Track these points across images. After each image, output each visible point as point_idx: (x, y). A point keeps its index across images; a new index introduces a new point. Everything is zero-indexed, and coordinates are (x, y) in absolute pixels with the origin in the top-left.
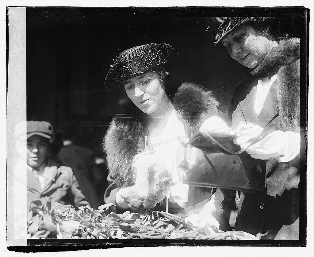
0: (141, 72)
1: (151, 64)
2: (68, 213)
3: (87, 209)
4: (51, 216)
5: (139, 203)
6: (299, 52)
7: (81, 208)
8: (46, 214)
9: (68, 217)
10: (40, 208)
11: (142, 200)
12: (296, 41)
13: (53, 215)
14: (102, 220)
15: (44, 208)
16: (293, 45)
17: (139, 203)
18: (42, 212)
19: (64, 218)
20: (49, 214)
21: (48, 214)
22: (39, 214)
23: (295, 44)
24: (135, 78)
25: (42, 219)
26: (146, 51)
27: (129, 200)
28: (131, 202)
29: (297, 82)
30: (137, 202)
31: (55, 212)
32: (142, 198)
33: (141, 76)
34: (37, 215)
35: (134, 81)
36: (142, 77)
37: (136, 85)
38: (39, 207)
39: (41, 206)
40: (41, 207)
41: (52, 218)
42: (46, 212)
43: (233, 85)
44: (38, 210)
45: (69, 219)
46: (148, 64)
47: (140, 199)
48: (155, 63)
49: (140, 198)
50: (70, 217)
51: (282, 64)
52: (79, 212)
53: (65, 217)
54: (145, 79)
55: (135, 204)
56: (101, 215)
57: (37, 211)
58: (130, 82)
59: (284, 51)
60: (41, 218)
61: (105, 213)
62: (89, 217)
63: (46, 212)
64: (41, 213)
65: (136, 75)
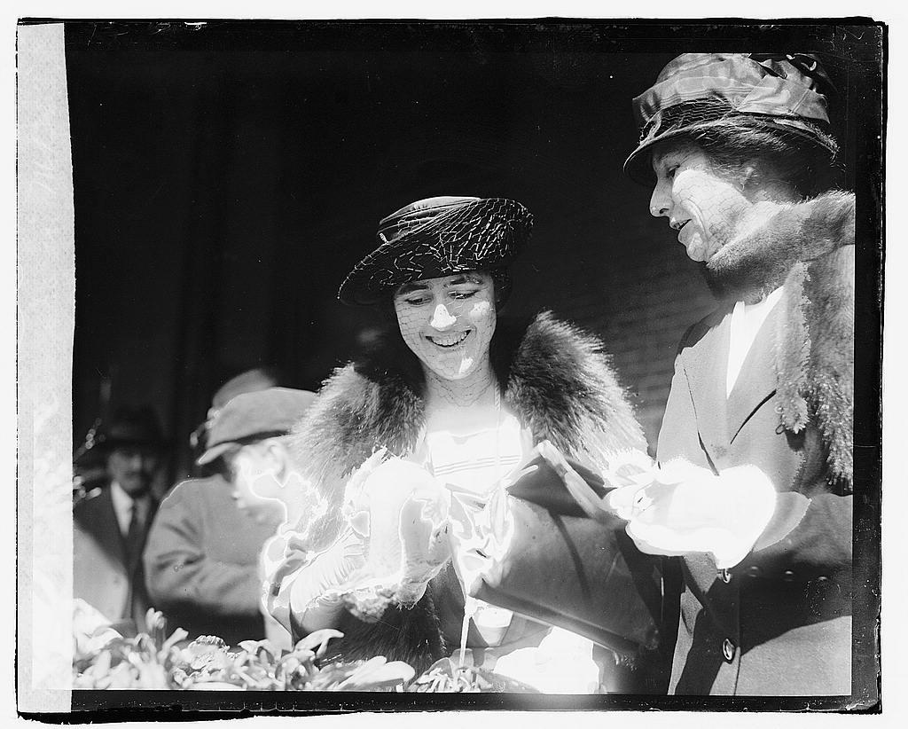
0: (466, 267)
1: (490, 250)
2: (209, 659)
3: (263, 653)
4: (162, 668)
5: (380, 605)
6: (850, 230)
7: (250, 644)
8: (149, 661)
9: (211, 672)
10: (131, 645)
11: (389, 595)
12: (843, 200)
13: (168, 663)
14: (304, 684)
15: (144, 644)
16: (836, 210)
17: (380, 605)
18: (138, 654)
19: (197, 673)
20: (158, 662)
21: (154, 662)
22: (127, 660)
23: (840, 207)
24: (443, 280)
25: (136, 676)
26: (474, 211)
27: (354, 598)
28: (358, 604)
29: (829, 305)
30: (375, 601)
31: (173, 659)
32: (389, 591)
33: (459, 278)
34: (123, 665)
35: (438, 286)
36: (462, 281)
37: (439, 296)
38: (130, 640)
39: (134, 637)
40: (135, 641)
41: (166, 673)
42: (150, 656)
43: (647, 296)
44: (127, 651)
45: (212, 678)
46: (484, 250)
47: (384, 595)
48: (498, 249)
49: (381, 590)
50: (213, 671)
51: (797, 256)
52: (242, 656)
53: (200, 671)
54: (465, 287)
55: (370, 609)
56: (302, 670)
57: (122, 653)
58: (424, 287)
59: (807, 221)
60: (134, 672)
61: (317, 663)
62: (270, 675)
63: (150, 656)
64: (134, 657)
65: (449, 273)
